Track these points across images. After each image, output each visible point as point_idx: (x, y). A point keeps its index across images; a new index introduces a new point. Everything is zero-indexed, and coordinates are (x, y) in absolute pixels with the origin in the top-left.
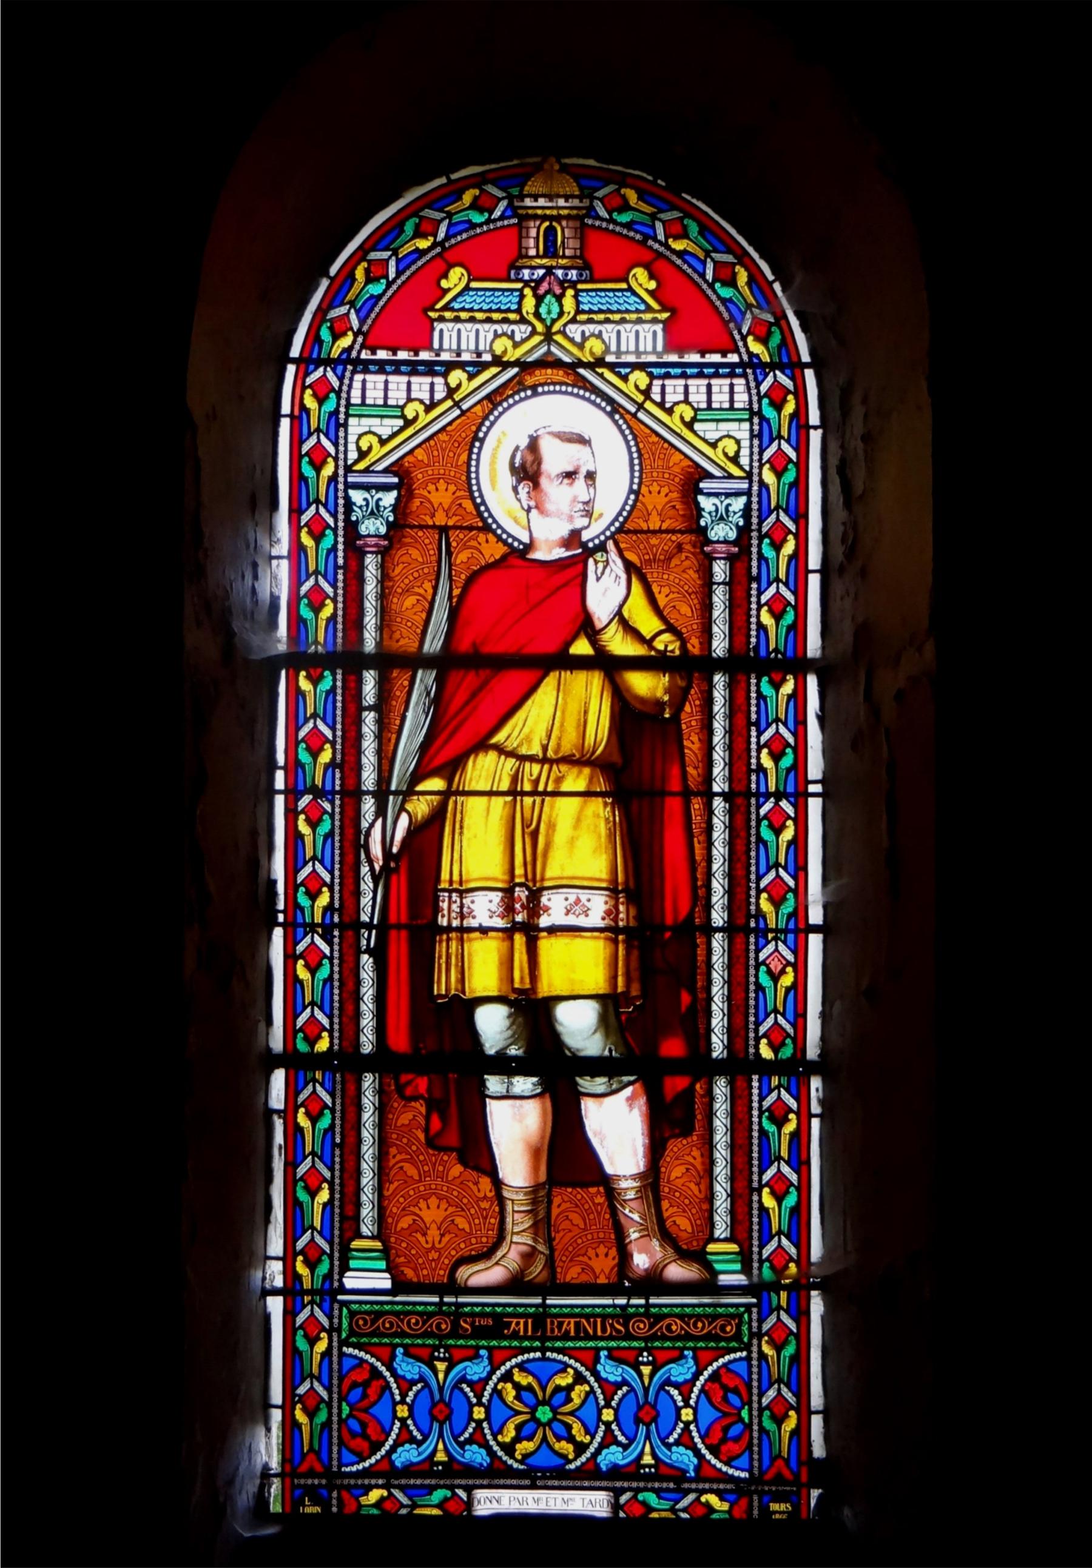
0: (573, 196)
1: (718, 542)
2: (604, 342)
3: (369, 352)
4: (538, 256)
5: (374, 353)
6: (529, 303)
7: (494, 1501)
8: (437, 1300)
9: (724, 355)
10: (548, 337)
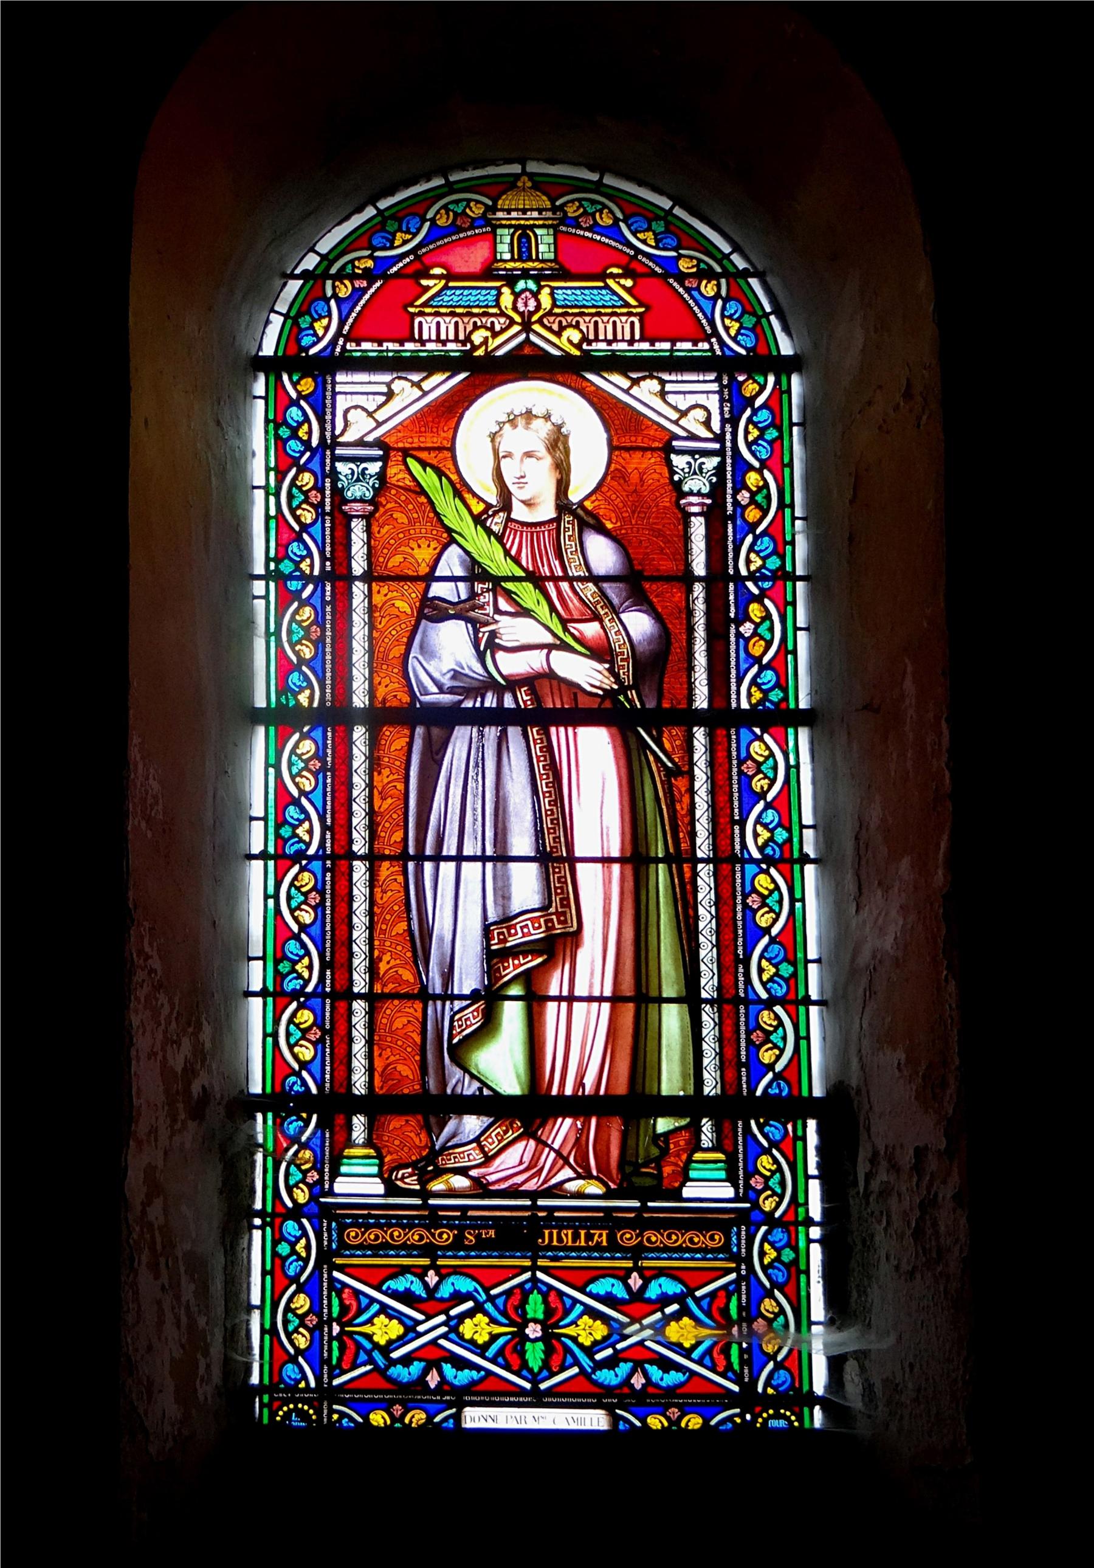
0: (546, 210)
1: (355, 501)
2: (581, 331)
3: (354, 344)
4: (512, 260)
5: (358, 345)
6: (507, 299)
7: (489, 1420)
8: (637, 1204)
9: (402, 345)
10: (527, 327)
